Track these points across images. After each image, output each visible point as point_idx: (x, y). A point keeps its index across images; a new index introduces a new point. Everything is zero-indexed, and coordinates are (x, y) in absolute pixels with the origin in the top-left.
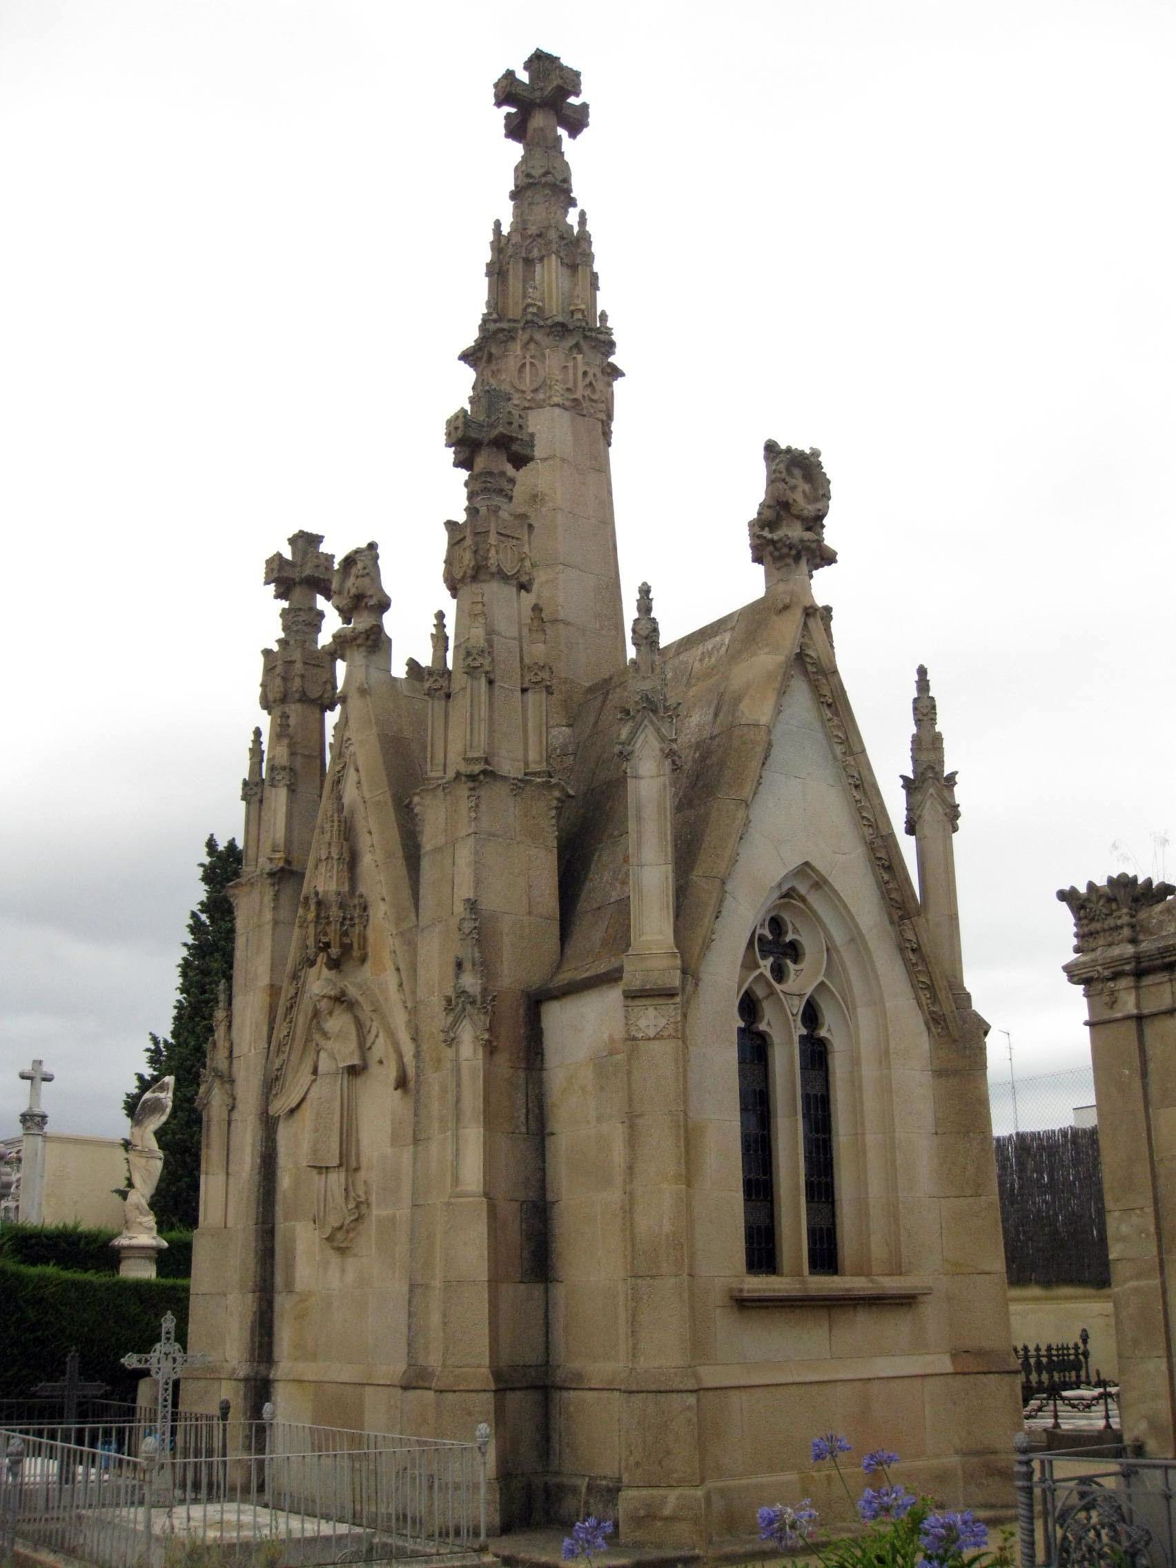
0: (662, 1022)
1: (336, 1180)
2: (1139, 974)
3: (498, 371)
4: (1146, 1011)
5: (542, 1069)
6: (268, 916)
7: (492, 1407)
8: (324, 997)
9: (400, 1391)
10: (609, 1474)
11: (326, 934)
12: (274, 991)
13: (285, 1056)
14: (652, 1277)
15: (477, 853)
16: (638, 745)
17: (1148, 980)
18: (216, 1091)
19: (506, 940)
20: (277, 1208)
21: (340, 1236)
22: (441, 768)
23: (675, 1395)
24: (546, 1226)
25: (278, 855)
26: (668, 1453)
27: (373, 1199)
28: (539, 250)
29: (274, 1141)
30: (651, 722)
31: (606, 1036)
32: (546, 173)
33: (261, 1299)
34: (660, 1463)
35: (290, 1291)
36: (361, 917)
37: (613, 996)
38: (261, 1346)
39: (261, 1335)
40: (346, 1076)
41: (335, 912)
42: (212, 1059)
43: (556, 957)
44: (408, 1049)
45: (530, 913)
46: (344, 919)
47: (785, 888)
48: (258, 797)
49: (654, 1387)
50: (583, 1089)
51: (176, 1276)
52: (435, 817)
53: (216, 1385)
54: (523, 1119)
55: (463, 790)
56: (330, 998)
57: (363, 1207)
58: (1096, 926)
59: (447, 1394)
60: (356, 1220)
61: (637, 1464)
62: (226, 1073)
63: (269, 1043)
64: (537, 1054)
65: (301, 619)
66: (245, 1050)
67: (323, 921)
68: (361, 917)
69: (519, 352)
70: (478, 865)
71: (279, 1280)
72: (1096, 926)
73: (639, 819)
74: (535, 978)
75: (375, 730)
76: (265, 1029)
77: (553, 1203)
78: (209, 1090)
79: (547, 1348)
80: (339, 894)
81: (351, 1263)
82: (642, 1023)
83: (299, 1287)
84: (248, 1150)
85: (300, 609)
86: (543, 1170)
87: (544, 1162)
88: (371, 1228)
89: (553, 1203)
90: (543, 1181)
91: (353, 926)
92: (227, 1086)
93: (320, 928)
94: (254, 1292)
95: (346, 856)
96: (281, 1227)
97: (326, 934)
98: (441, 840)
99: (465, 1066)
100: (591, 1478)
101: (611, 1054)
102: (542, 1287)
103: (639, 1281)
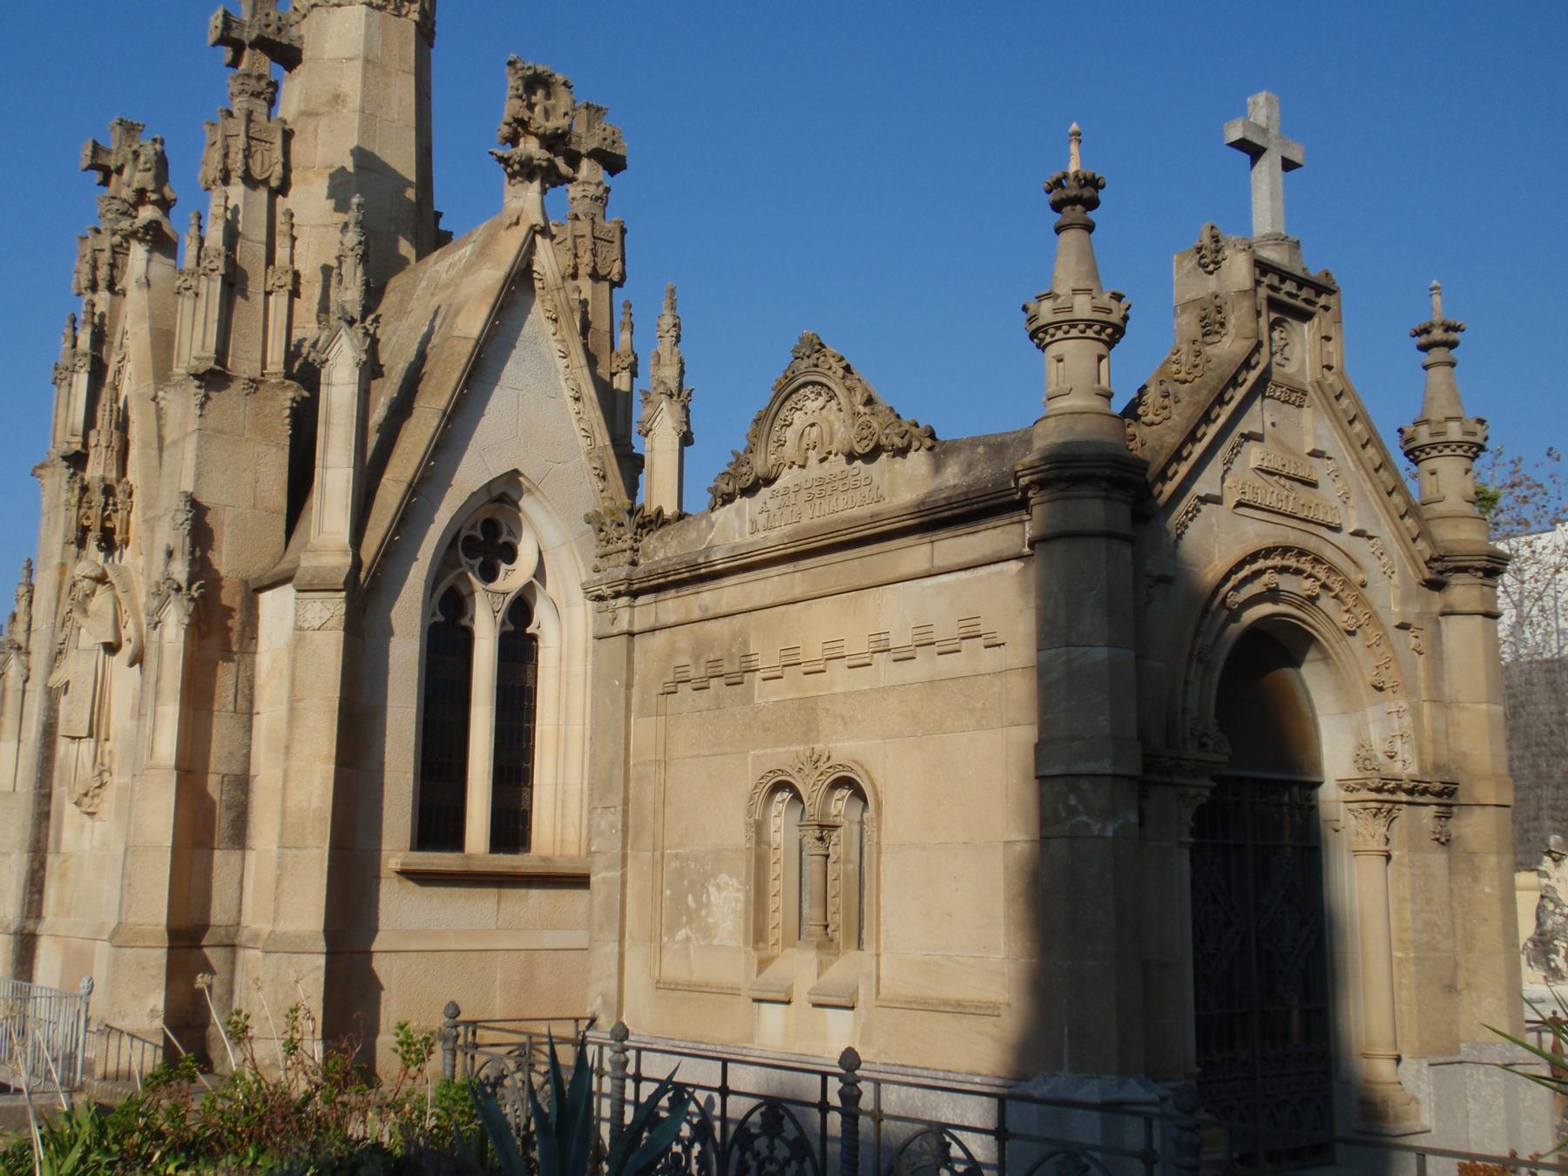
1: (87, 746)
2: (635, 595)
4: (636, 628)
5: (255, 653)
7: (164, 961)
17: (642, 600)
18: (13, 662)
19: (227, 531)
21: (86, 801)
27: (115, 768)
29: (56, 711)
33: (33, 860)
35: (58, 852)
37: (288, 591)
38: (30, 903)
39: (31, 893)
45: (254, 507)
47: (495, 493)
54: (231, 698)
57: (106, 775)
58: (610, 548)
65: (115, 207)
70: (200, 461)
72: (610, 548)
74: (257, 567)
75: (146, 325)
80: (103, 479)
82: (309, 615)
83: (63, 849)
84: (35, 718)
90: (248, 757)
91: (116, 511)
99: (167, 647)
102: (238, 853)
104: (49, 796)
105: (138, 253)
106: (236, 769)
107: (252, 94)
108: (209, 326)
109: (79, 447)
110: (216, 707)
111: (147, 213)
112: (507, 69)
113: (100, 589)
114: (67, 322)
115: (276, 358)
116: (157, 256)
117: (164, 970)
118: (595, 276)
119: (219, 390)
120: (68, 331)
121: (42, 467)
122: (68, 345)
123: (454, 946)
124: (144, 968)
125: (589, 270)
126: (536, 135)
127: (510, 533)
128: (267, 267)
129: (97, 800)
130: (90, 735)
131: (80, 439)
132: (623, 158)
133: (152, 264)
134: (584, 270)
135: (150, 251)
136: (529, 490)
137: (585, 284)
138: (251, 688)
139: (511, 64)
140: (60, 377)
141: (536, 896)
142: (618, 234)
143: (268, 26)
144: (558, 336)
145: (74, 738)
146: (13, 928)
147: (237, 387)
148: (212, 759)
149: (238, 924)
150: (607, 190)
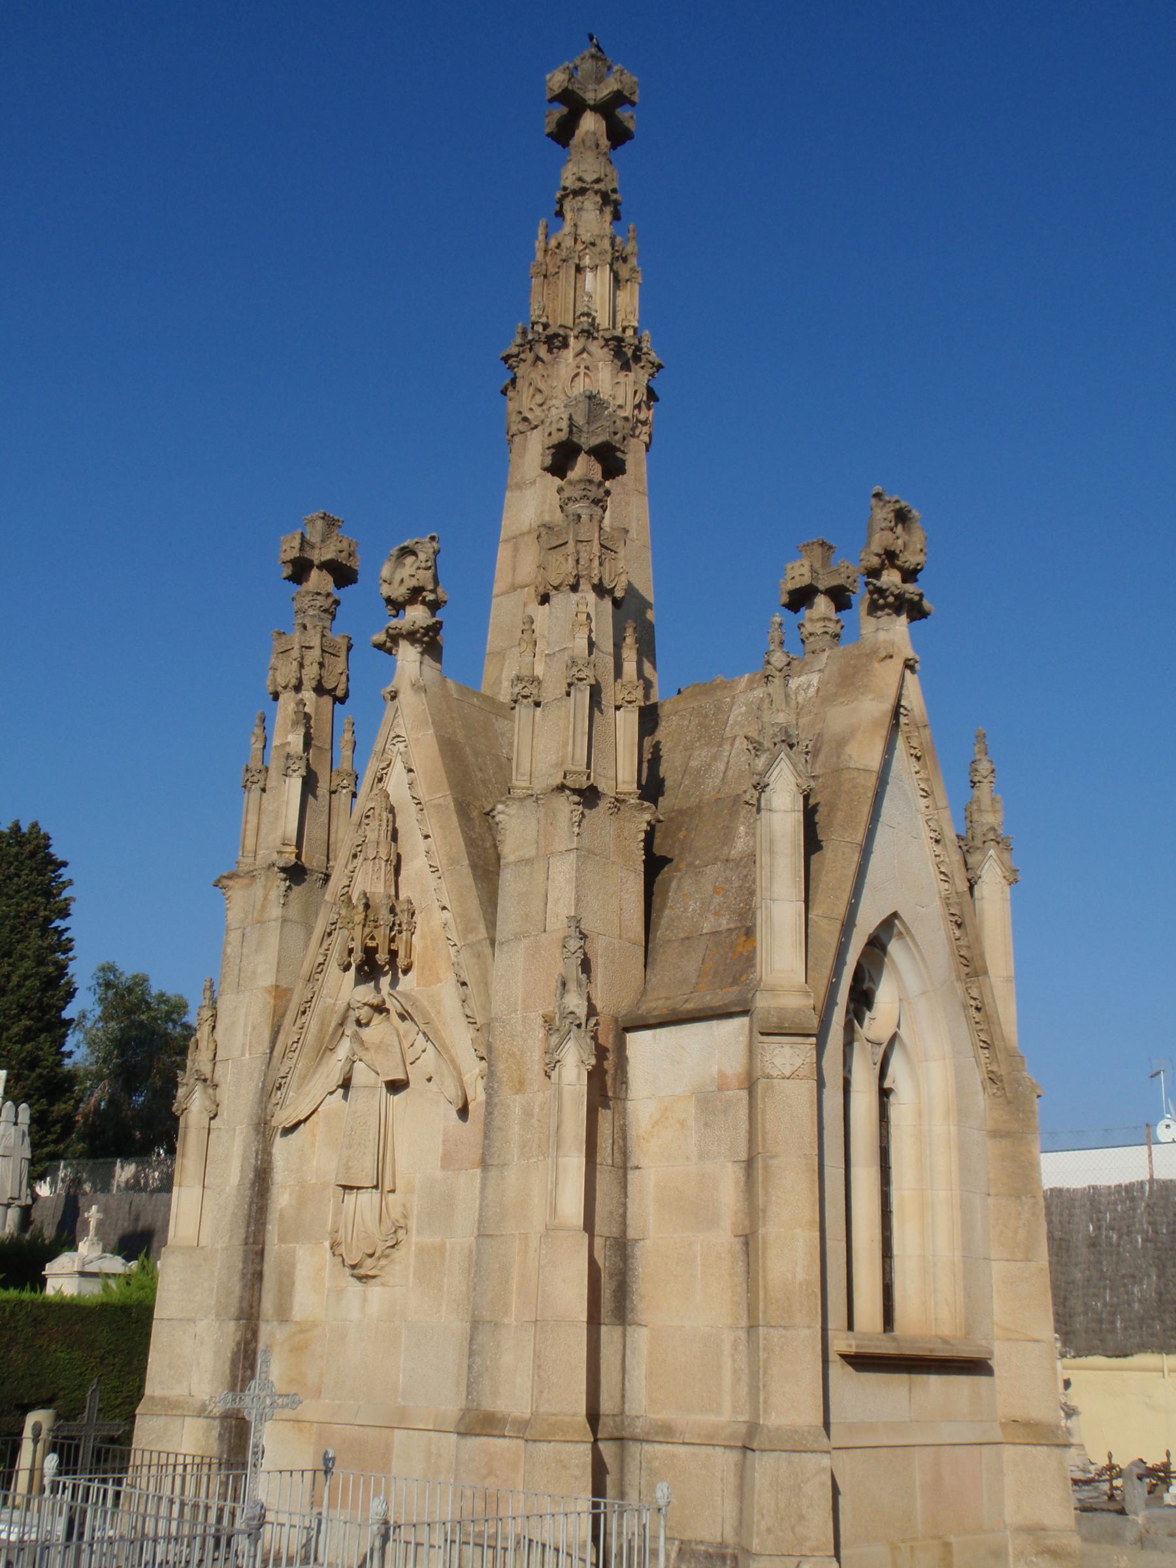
0: (798, 1062)
3: (548, 376)
5: (625, 1099)
6: (275, 912)
8: (365, 1004)
9: (454, 1437)
10: (707, 1538)
11: (373, 938)
12: (280, 993)
13: (292, 1063)
14: (784, 1327)
15: (578, 870)
16: (772, 778)
19: (600, 961)
20: (269, 1227)
22: (527, 778)
23: (809, 1455)
24: (625, 1265)
25: (289, 849)
26: (801, 1517)
27: (413, 1224)
28: (591, 258)
29: (270, 1154)
30: (788, 756)
31: (715, 1069)
32: (598, 181)
33: (247, 1328)
34: (793, 1529)
36: (409, 923)
40: (384, 1090)
41: (384, 916)
42: (194, 1061)
43: (639, 982)
44: (473, 1070)
46: (394, 924)
48: (261, 784)
49: (788, 1447)
50: (682, 1123)
51: (20, 1286)
52: (517, 829)
53: (179, 1421)
54: (609, 1148)
55: (565, 806)
56: (371, 1006)
57: (401, 1232)
59: (538, 1444)
60: (393, 1247)
61: (769, 1530)
62: (208, 1076)
63: (272, 1049)
64: (623, 1083)
66: (237, 1054)
67: (372, 924)
68: (409, 923)
69: (571, 360)
70: (579, 886)
71: (268, 1304)
73: (771, 852)
75: (431, 732)
76: (266, 1035)
77: (636, 1241)
78: (191, 1092)
79: (623, 1396)
81: (375, 1291)
82: (778, 1061)
83: (297, 1314)
85: (318, 594)
86: (625, 1205)
87: (626, 1196)
88: (407, 1255)
89: (636, 1241)
90: (624, 1216)
91: (400, 932)
92: (210, 1091)
93: (367, 930)
94: (238, 1319)
95: (393, 857)
96: (274, 1246)
97: (373, 938)
98: (530, 852)
99: (567, 1092)
100: (682, 1542)
101: (720, 1089)
102: (620, 1328)
103: (771, 1330)
104: (261, 1253)
105: (408, 656)
106: (616, 1231)
107: (593, 501)
108: (578, 738)
109: (293, 858)
110: (598, 1161)
111: (417, 615)
112: (873, 501)
113: (377, 1018)
114: (257, 722)
115: (627, 777)
116: (427, 659)
117: (589, 1469)
118: (320, 690)
119: (591, 808)
120: (258, 731)
121: (230, 877)
122: (259, 745)
123: (886, 1441)
124: (565, 1467)
125: (314, 683)
126: (900, 569)
127: (871, 979)
128: (615, 680)
129: (383, 1262)
130: (376, 1187)
131: (293, 849)
132: (355, 573)
133: (424, 666)
134: (308, 684)
135: (422, 653)
136: (900, 933)
137: (308, 695)
138: (624, 1139)
139: (877, 496)
140: (255, 778)
141: (934, 1381)
142: (344, 648)
143: (615, 433)
144: (922, 775)
145: (351, 1188)
146: (217, 1411)
147: (604, 804)
148: (597, 1219)
149: (622, 1412)
150: (337, 603)
